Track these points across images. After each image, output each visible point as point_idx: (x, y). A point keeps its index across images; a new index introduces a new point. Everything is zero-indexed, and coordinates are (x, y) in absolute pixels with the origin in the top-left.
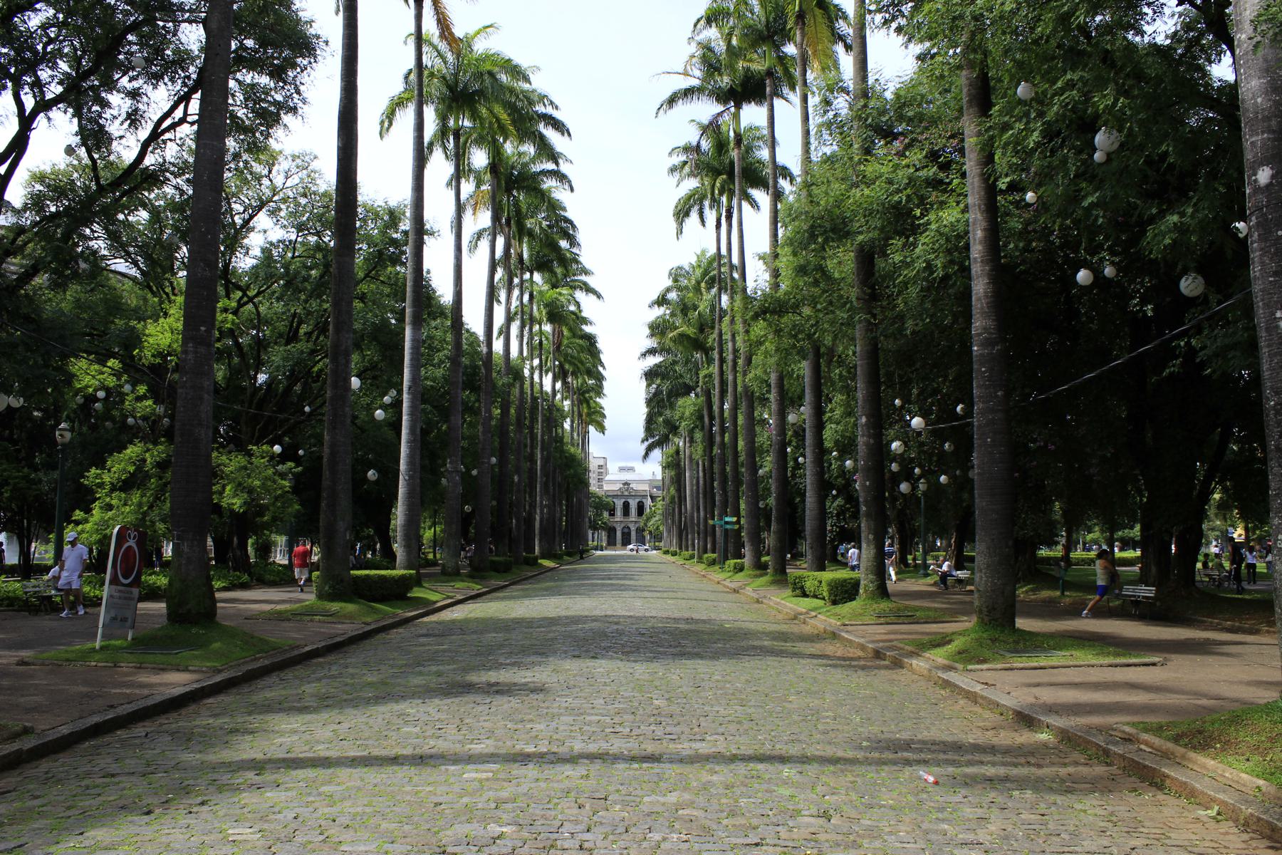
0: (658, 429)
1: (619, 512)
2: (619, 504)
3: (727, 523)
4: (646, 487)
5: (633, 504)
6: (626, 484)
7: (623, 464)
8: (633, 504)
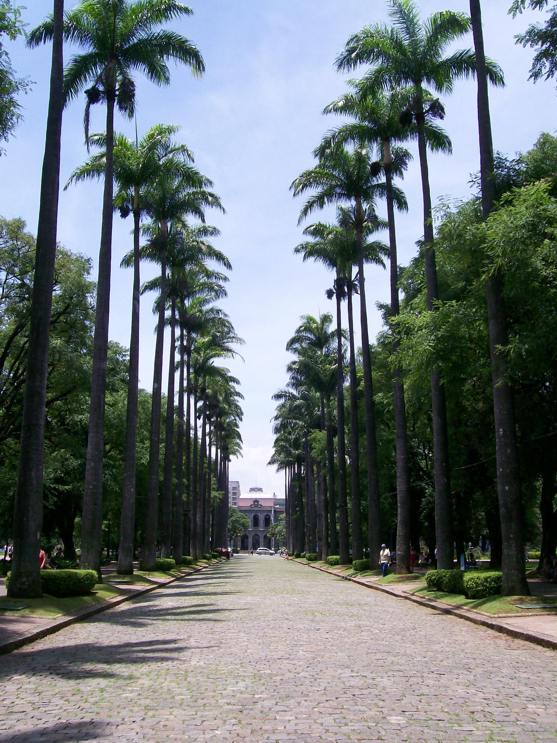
5: (262, 517)
7: (253, 486)
8: (262, 517)
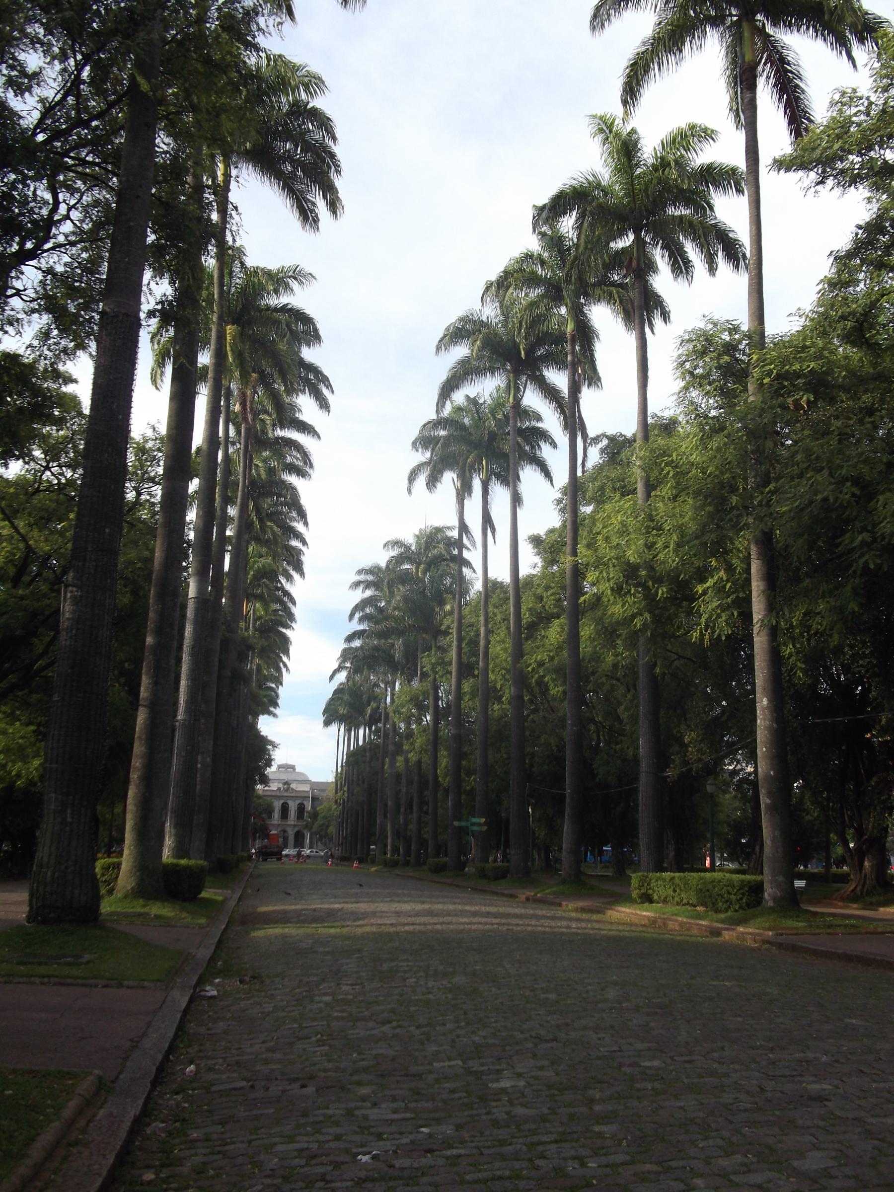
0: (345, 708)
1: (276, 815)
2: (277, 805)
3: (473, 824)
4: (307, 788)
5: (293, 806)
6: (286, 783)
8: (293, 806)
